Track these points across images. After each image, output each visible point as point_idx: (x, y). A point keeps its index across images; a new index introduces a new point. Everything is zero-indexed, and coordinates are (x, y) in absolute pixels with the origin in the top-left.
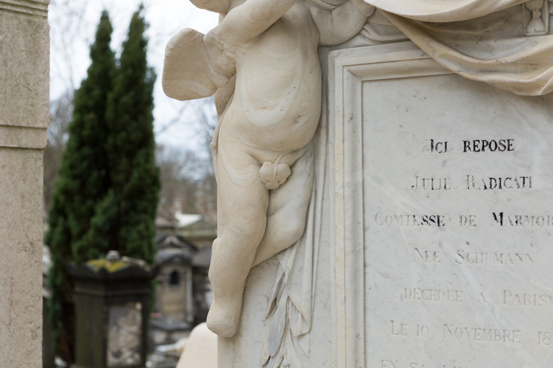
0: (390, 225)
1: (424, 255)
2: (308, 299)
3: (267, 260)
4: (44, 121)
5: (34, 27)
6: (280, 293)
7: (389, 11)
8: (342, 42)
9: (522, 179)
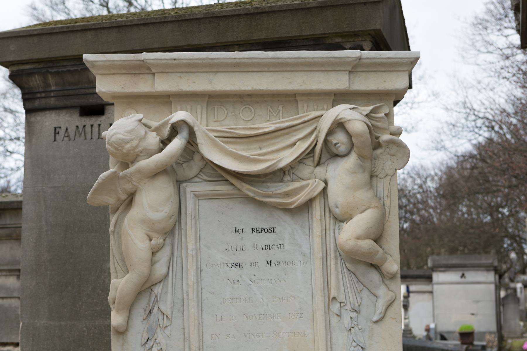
1: (233, 282)
9: (280, 245)
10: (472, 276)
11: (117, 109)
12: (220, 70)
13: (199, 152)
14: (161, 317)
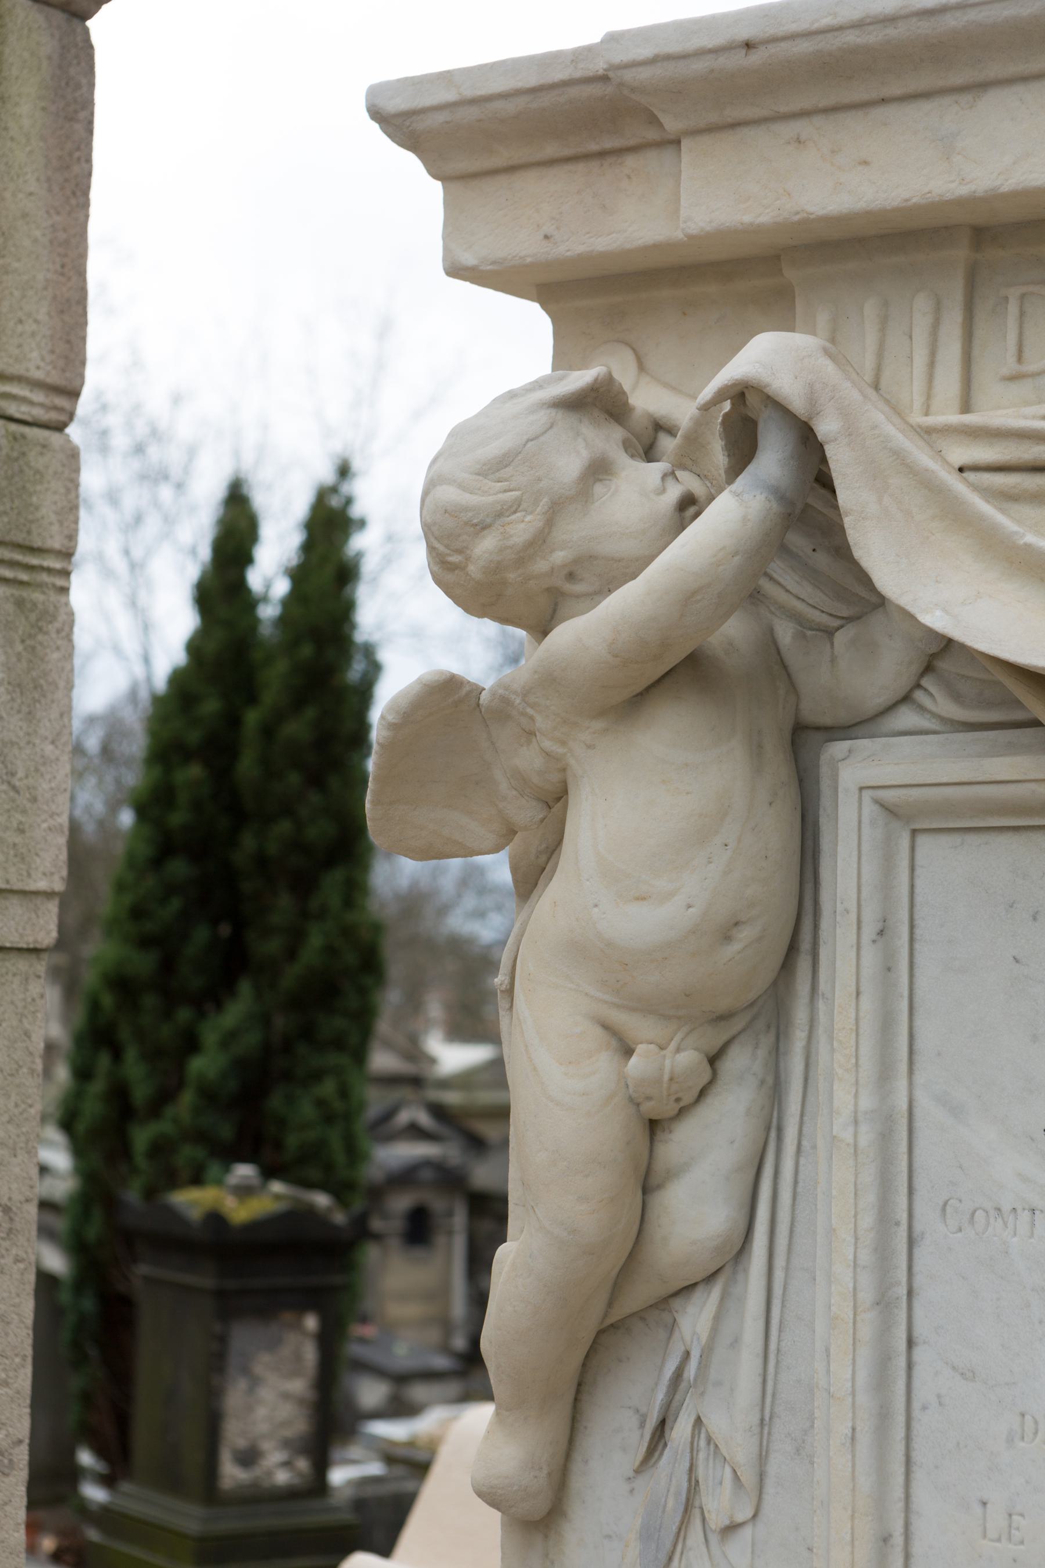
0: (983, 1234)
2: (751, 1427)
3: (641, 1310)
4: (52, 874)
5: (33, 617)
6: (675, 1404)
7: (986, 652)
8: (859, 720)
12: (994, 70)
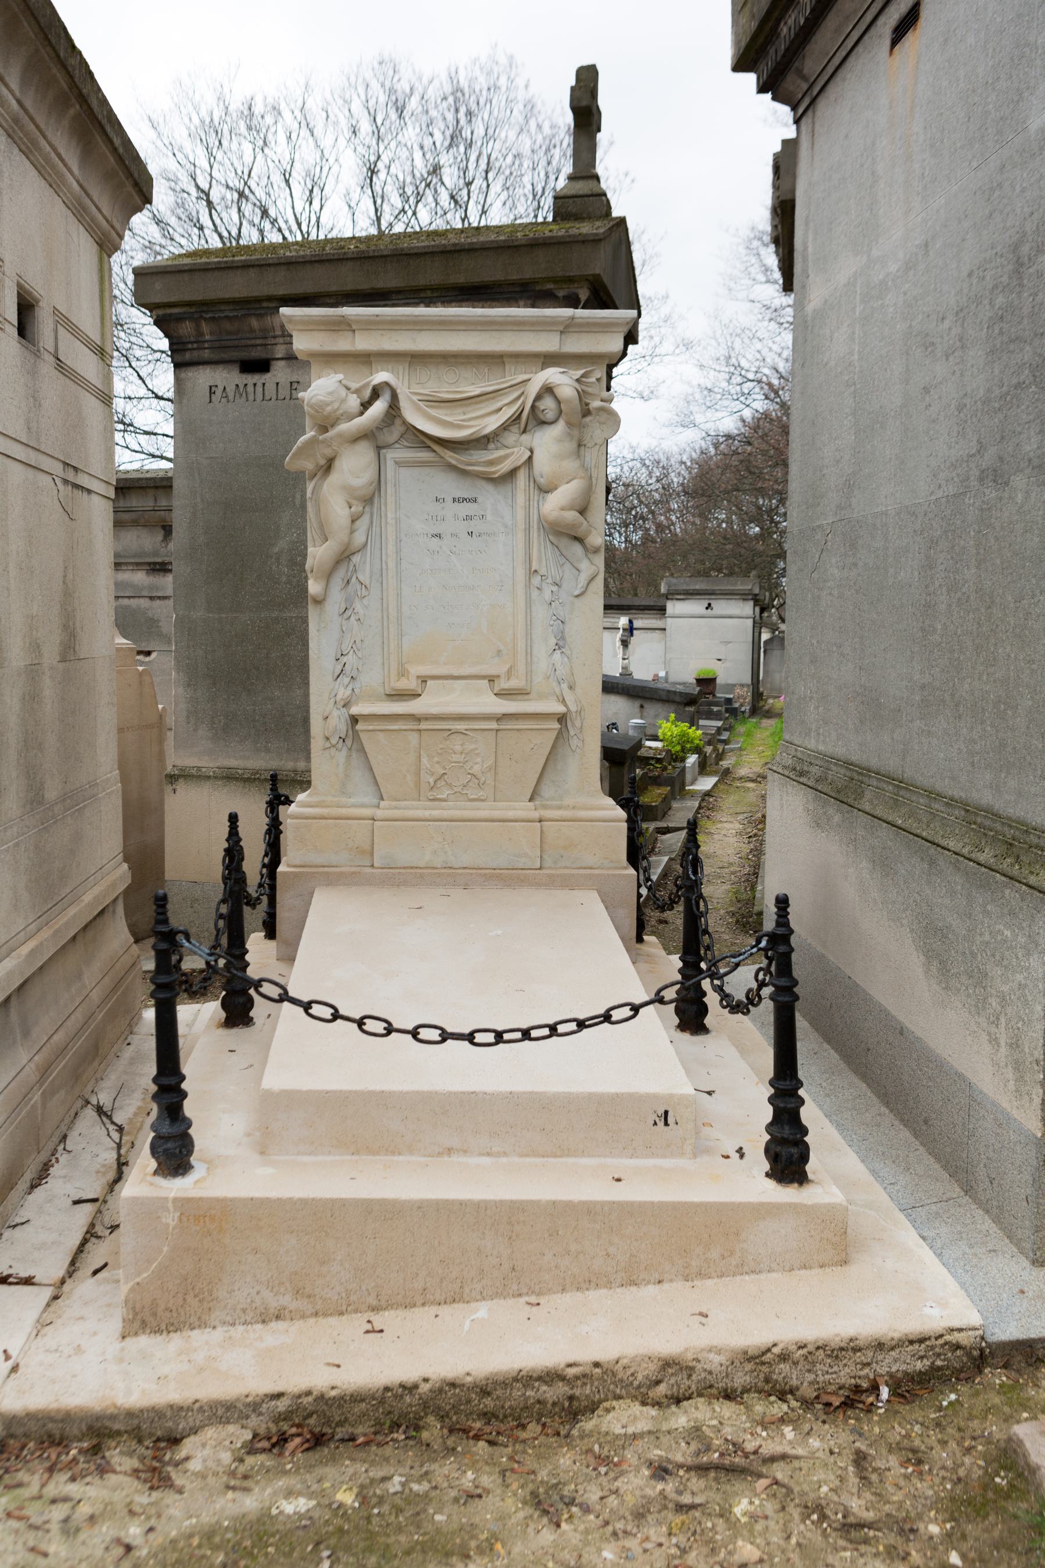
10: (721, 606)
11: (314, 369)
13: (400, 416)
14: (359, 587)
